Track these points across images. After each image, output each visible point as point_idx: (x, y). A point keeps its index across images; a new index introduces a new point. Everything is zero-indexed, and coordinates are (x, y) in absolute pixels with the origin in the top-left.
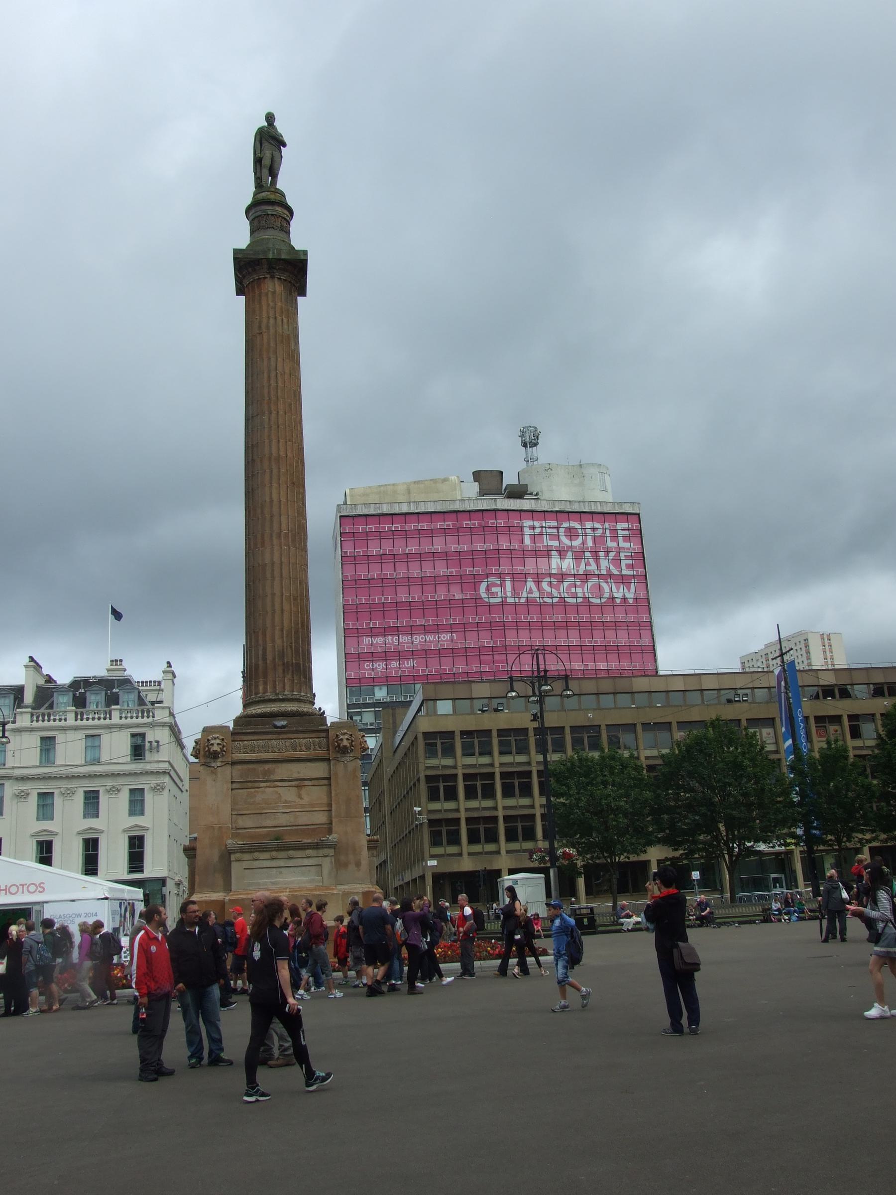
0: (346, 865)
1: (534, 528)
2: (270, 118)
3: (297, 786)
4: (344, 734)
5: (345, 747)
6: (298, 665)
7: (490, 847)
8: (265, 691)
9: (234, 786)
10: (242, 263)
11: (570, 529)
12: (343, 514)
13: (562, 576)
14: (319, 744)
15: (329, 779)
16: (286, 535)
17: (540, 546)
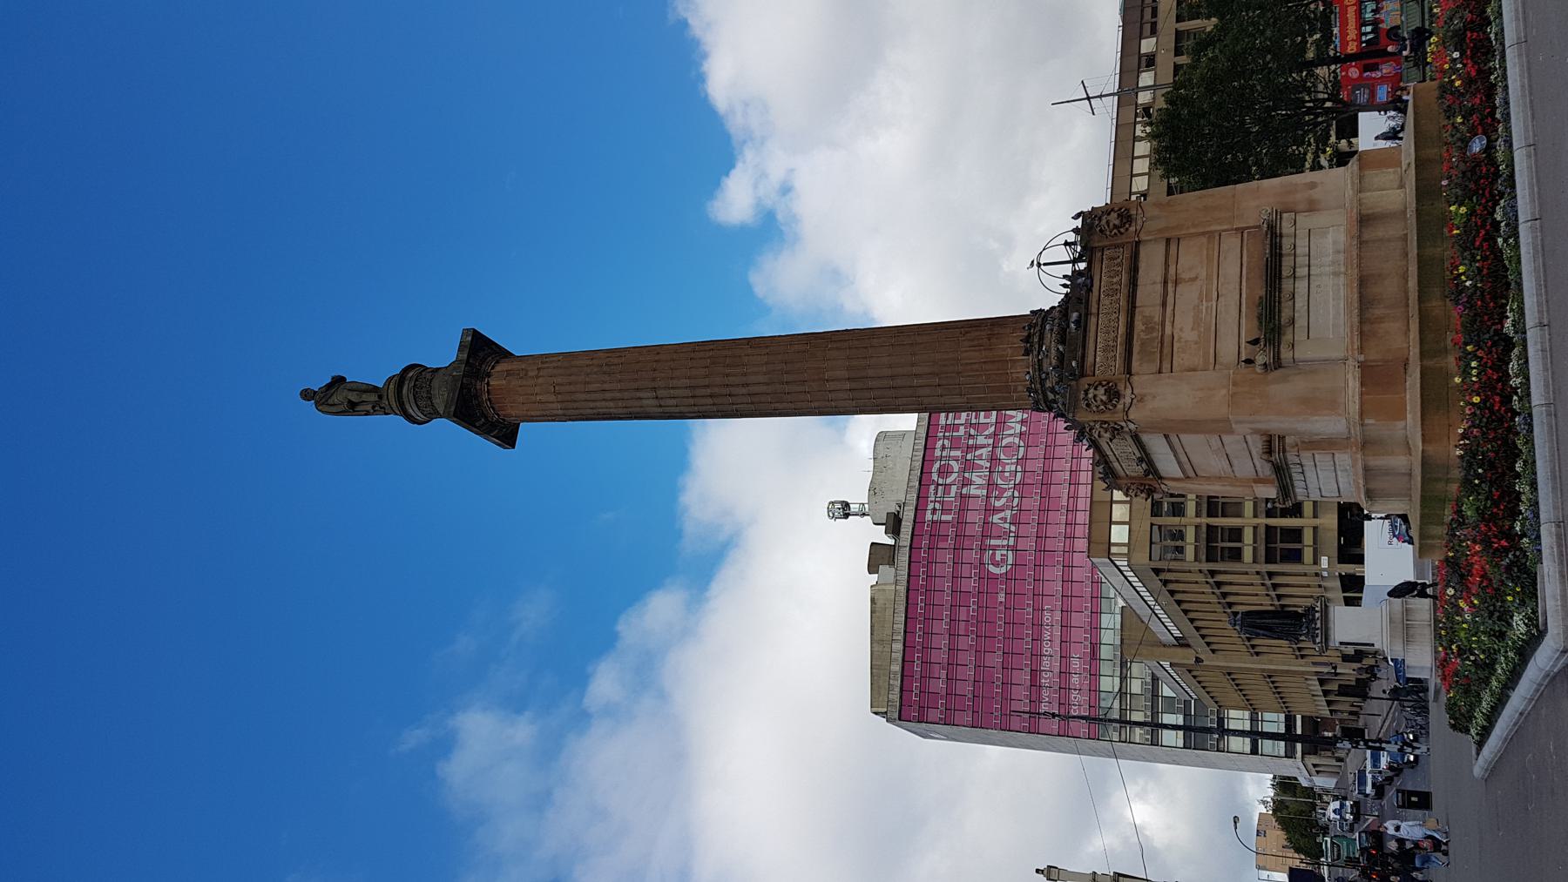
1: (934, 510)
2: (307, 395)
3: (1176, 283)
7: (1308, 538)
9: (1166, 366)
11: (940, 473)
12: (896, 715)
13: (991, 485)
17: (955, 505)
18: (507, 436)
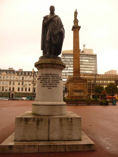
0: (85, 93)
18: (72, 30)
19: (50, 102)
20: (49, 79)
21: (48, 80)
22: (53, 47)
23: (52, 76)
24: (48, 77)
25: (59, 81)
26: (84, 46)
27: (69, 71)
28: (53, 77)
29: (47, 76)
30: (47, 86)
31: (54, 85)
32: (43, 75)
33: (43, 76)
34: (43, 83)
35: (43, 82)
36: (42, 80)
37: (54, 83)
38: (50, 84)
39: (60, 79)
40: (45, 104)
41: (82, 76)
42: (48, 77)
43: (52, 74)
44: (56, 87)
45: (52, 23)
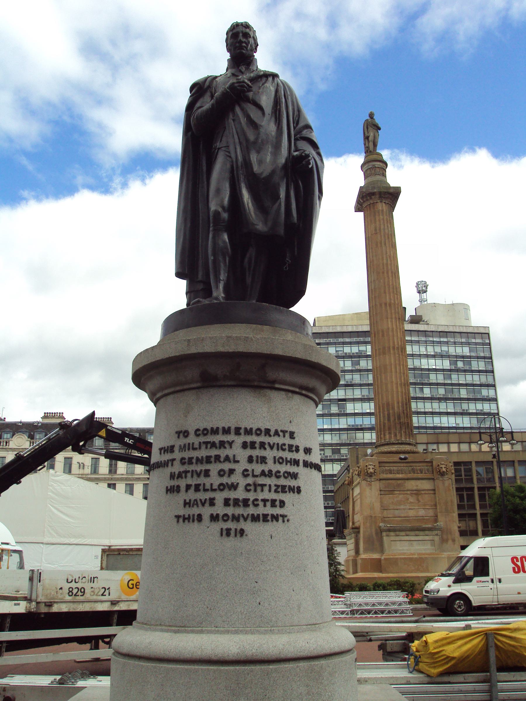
0: (447, 541)
2: (371, 116)
4: (442, 464)
5: (444, 472)
6: (408, 423)
8: (390, 438)
9: (382, 492)
10: (364, 194)
14: (428, 470)
15: (434, 490)
16: (398, 348)
18: (358, 209)
19: (236, 632)
20: (226, 466)
21: (221, 473)
22: (252, 252)
23: (245, 445)
24: (222, 453)
25: (295, 476)
26: (422, 289)
27: (351, 421)
28: (257, 453)
29: (213, 445)
30: (214, 518)
31: (261, 510)
32: (183, 441)
33: (183, 448)
34: (183, 496)
35: (183, 488)
36: (180, 476)
37: (266, 495)
38: (236, 502)
39: (306, 464)
40: (198, 654)
41: (424, 447)
42: (222, 453)
43: (249, 432)
44: (275, 518)
45: (242, 109)
